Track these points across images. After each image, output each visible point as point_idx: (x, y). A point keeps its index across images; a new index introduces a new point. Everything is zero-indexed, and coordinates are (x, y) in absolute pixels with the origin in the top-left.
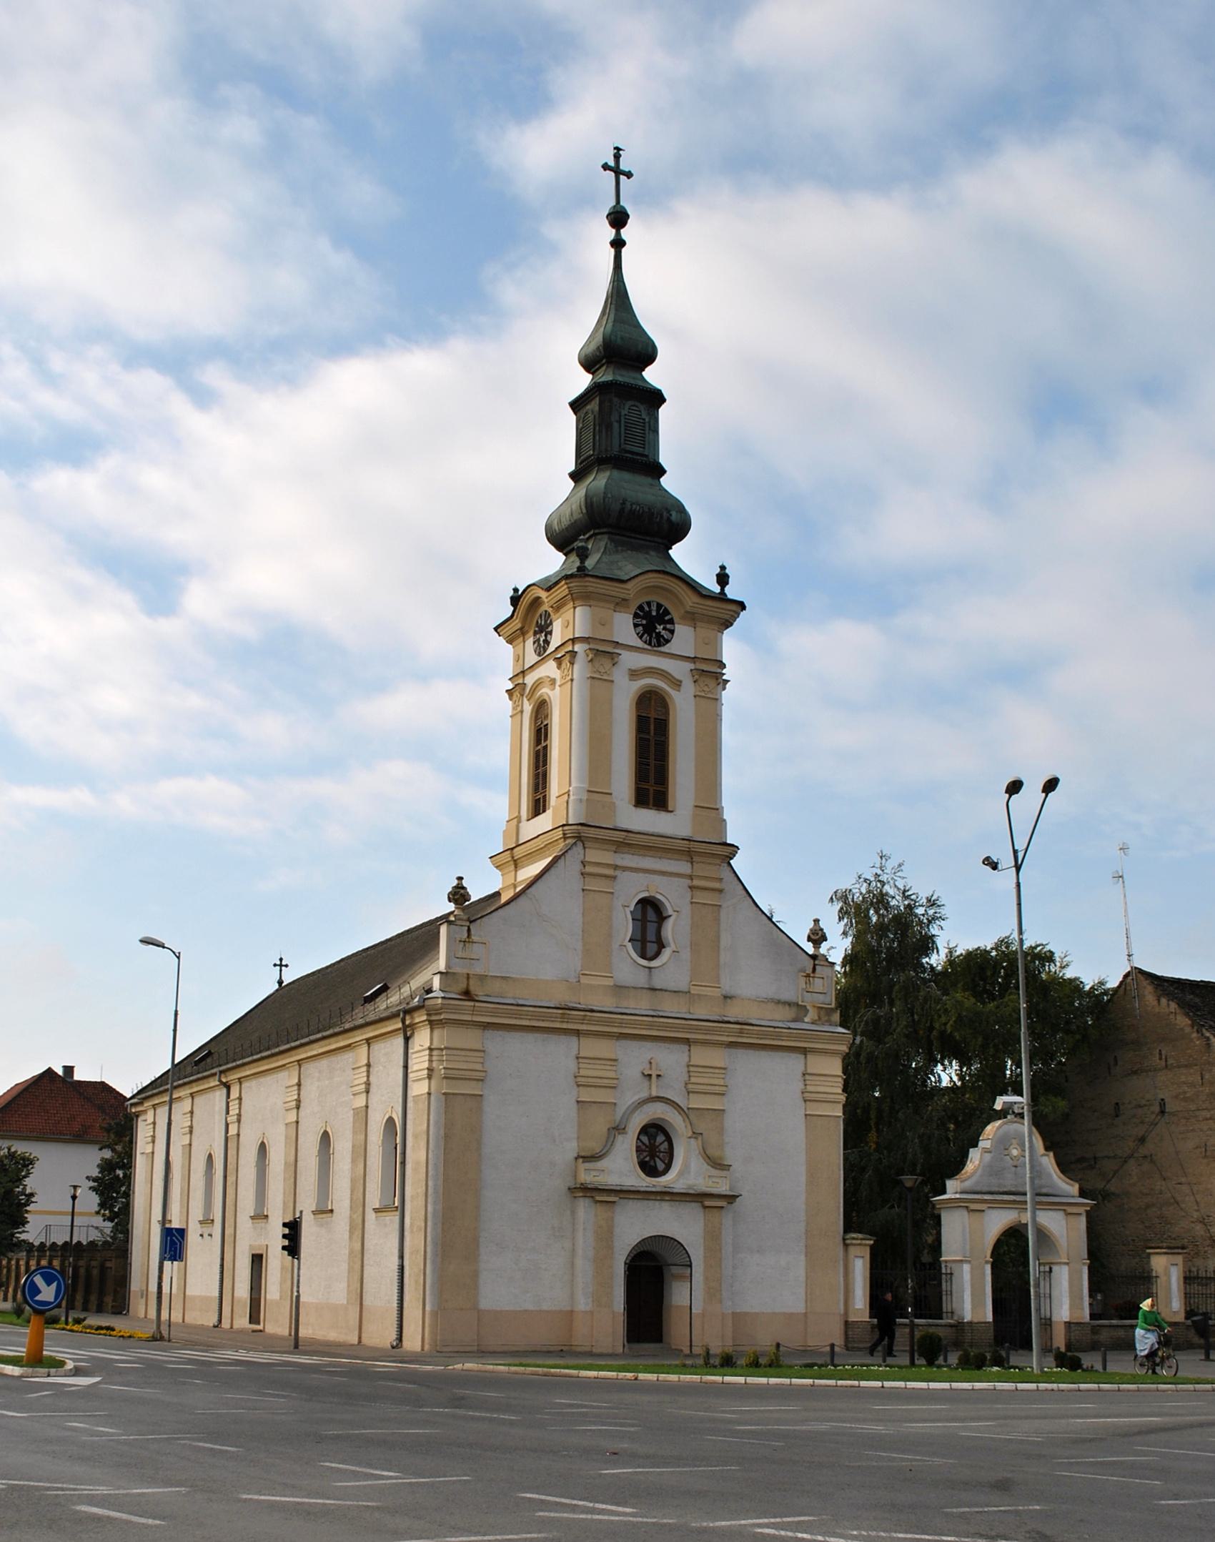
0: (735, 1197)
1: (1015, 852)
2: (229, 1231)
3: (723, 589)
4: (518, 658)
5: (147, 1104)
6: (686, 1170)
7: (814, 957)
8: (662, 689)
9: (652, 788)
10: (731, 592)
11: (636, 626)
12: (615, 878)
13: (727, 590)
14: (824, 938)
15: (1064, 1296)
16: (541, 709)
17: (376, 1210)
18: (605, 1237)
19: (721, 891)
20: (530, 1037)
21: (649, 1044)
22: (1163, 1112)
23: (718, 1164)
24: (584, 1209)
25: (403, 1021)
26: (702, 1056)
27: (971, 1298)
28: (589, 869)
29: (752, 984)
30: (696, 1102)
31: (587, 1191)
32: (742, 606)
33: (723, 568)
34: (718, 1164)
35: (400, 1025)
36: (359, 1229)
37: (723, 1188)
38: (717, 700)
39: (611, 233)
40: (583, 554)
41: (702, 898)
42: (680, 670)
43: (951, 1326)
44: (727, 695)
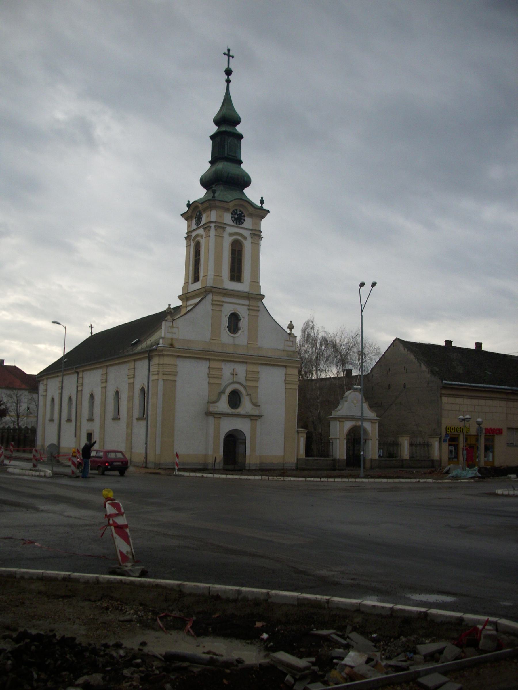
0: (261, 416)
1: (361, 305)
2: (78, 424)
3: (262, 205)
4: (189, 226)
5: (44, 378)
6: (246, 407)
7: (290, 334)
8: (240, 240)
9: (236, 274)
10: (265, 207)
11: (232, 217)
12: (222, 305)
13: (263, 205)
14: (293, 328)
15: (372, 450)
16: (198, 246)
17: (137, 419)
18: (217, 430)
19: (259, 311)
20: (193, 361)
21: (233, 364)
22: (405, 387)
23: (256, 405)
24: (211, 420)
25: (149, 354)
26: (251, 368)
27: (340, 451)
28: (214, 302)
29: (268, 344)
30: (249, 384)
31: (209, 414)
32: (268, 211)
33: (262, 198)
34: (256, 405)
35: (147, 355)
36: (130, 425)
37: (257, 413)
38: (259, 244)
39: (226, 77)
40: (214, 192)
41: (252, 313)
42: (246, 233)
43: (332, 460)
44: (263, 243)
